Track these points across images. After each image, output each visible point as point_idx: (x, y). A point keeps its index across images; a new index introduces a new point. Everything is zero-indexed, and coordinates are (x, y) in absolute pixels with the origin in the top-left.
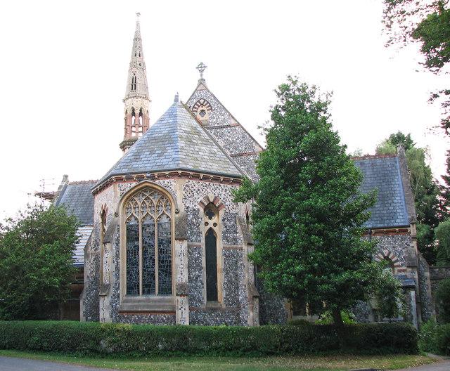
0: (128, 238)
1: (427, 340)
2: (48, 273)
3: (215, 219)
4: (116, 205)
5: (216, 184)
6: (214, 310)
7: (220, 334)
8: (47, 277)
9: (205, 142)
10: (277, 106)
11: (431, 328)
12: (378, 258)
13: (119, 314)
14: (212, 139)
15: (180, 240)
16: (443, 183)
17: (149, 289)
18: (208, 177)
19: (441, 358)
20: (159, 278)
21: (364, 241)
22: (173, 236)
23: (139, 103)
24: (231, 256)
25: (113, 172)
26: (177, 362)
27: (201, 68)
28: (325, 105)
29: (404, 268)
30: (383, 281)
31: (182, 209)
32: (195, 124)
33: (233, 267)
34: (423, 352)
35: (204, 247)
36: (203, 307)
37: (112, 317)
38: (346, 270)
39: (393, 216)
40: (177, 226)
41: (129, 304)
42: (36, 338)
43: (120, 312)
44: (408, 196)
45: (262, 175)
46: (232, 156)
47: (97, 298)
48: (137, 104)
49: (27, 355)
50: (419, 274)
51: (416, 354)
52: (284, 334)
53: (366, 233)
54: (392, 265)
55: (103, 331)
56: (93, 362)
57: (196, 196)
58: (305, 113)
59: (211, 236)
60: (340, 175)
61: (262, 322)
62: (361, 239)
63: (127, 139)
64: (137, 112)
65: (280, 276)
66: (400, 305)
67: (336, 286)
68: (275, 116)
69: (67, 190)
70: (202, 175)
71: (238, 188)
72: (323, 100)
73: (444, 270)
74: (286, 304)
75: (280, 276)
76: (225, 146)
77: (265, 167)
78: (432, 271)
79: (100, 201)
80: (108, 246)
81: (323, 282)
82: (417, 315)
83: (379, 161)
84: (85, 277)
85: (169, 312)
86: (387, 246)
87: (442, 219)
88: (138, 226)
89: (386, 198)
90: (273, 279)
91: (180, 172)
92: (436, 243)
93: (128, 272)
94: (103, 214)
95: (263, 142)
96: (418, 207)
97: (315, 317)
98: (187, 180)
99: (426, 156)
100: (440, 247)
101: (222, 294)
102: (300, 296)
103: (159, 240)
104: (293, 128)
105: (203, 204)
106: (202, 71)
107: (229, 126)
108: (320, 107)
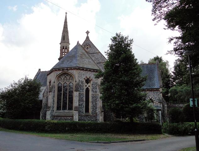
0: (58, 90)
1: (165, 129)
2: (28, 103)
3: (89, 84)
4: (54, 79)
5: (90, 72)
6: (87, 116)
7: (89, 125)
8: (27, 104)
9: (87, 58)
10: (112, 44)
11: (167, 125)
12: (148, 99)
13: (53, 117)
14: (90, 57)
15: (76, 91)
16: (172, 74)
17: (64, 108)
18: (87, 70)
19: (170, 136)
20: (68, 105)
21: (142, 93)
22: (74, 90)
23: (66, 44)
24: (94, 97)
25: (54, 68)
26: (72, 135)
27: (88, 32)
28: (130, 44)
29: (157, 103)
30: (149, 107)
31: (78, 81)
32: (84, 51)
33: (95, 101)
34: (163, 133)
35: (85, 94)
36: (84, 114)
37: (51, 118)
38: (135, 103)
39: (154, 85)
40: (75, 86)
41: (57, 113)
42: (22, 126)
43: (54, 116)
44: (159, 78)
45: (105, 69)
46: (97, 63)
47: (46, 111)
48: (65, 45)
49: (18, 132)
50: (163, 105)
51: (161, 134)
52: (112, 125)
53: (144, 90)
54: (153, 102)
55: (46, 123)
56: (41, 135)
57: (83, 76)
58: (122, 47)
59: (87, 90)
60: (134, 69)
61: (105, 120)
62: (141, 92)
63: (61, 57)
64: (65, 48)
65: (110, 105)
66: (155, 116)
67: (131, 109)
68: (111, 47)
69: (40, 74)
70: (85, 69)
71: (96, 74)
72: (129, 42)
73: (172, 104)
74: (113, 115)
75: (110, 105)
76: (95, 60)
77: (107, 66)
78: (167, 104)
79: (49, 78)
80: (51, 93)
81: (126, 107)
82: (162, 120)
83: (149, 66)
84: (43, 104)
85: (71, 116)
86: (151, 95)
87: (172, 87)
88: (73, 86)
89: (151, 79)
90: (108, 105)
91: (77, 68)
92: (169, 95)
93: (57, 102)
94: (50, 82)
95: (106, 57)
96: (163, 82)
97: (124, 119)
98: (80, 71)
99: (167, 65)
100: (171, 96)
101: (90, 110)
102: (118, 112)
103: (69, 91)
104: (117, 53)
105: (85, 79)
106: (88, 34)
107: (97, 53)
108: (128, 45)
